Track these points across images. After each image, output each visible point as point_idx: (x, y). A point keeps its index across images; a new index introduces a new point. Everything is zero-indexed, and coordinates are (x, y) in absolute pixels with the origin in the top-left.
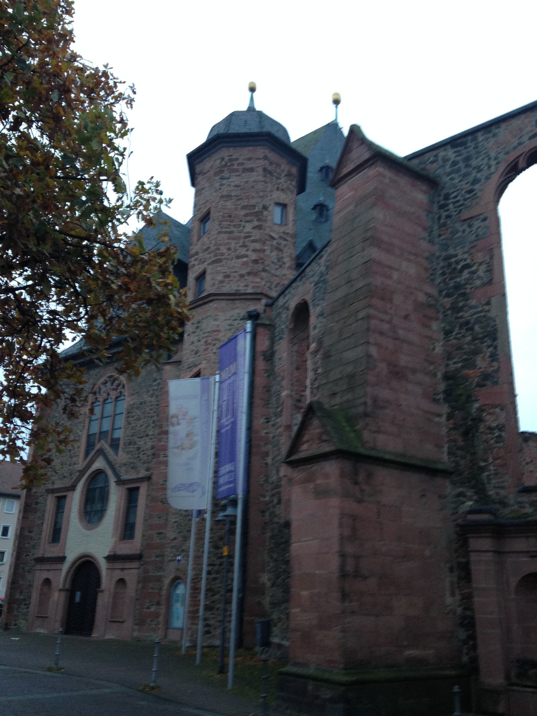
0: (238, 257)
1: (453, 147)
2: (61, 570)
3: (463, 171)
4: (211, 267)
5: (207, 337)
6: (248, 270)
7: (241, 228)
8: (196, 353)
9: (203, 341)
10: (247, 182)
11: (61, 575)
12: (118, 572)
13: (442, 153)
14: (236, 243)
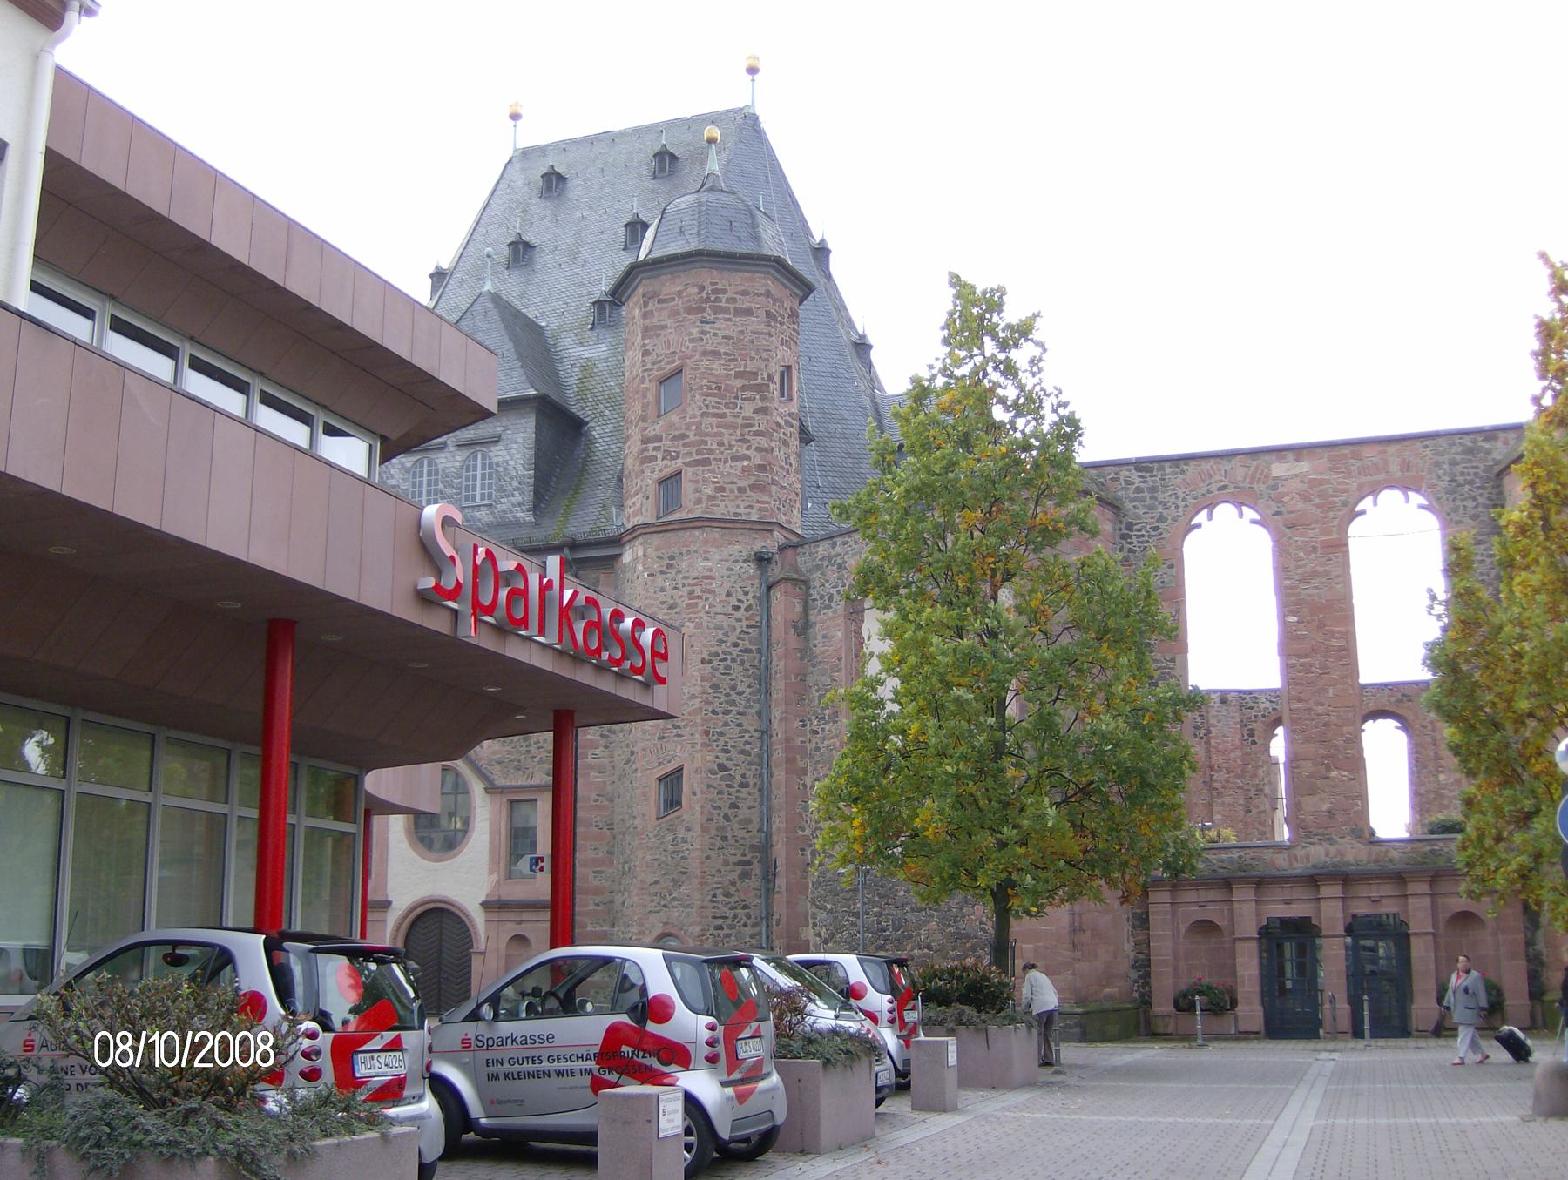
0: (735, 458)
1: (1138, 470)
2: (385, 921)
3: (1149, 502)
4: (690, 470)
5: (694, 585)
6: (752, 480)
7: (738, 410)
8: (671, 608)
9: (685, 591)
10: (742, 332)
11: (385, 928)
12: (512, 925)
13: (1124, 473)
14: (731, 435)
